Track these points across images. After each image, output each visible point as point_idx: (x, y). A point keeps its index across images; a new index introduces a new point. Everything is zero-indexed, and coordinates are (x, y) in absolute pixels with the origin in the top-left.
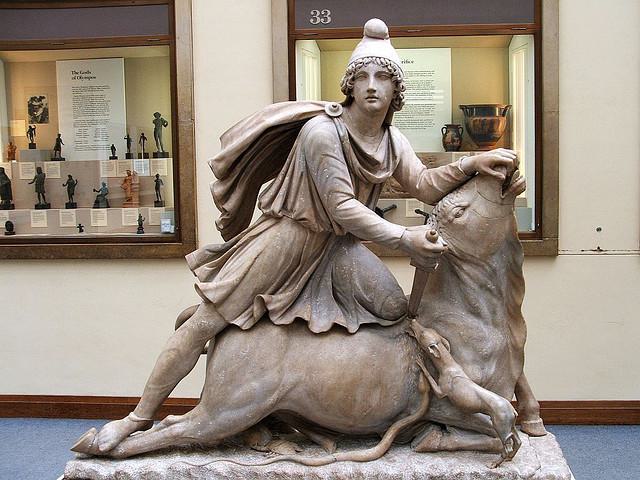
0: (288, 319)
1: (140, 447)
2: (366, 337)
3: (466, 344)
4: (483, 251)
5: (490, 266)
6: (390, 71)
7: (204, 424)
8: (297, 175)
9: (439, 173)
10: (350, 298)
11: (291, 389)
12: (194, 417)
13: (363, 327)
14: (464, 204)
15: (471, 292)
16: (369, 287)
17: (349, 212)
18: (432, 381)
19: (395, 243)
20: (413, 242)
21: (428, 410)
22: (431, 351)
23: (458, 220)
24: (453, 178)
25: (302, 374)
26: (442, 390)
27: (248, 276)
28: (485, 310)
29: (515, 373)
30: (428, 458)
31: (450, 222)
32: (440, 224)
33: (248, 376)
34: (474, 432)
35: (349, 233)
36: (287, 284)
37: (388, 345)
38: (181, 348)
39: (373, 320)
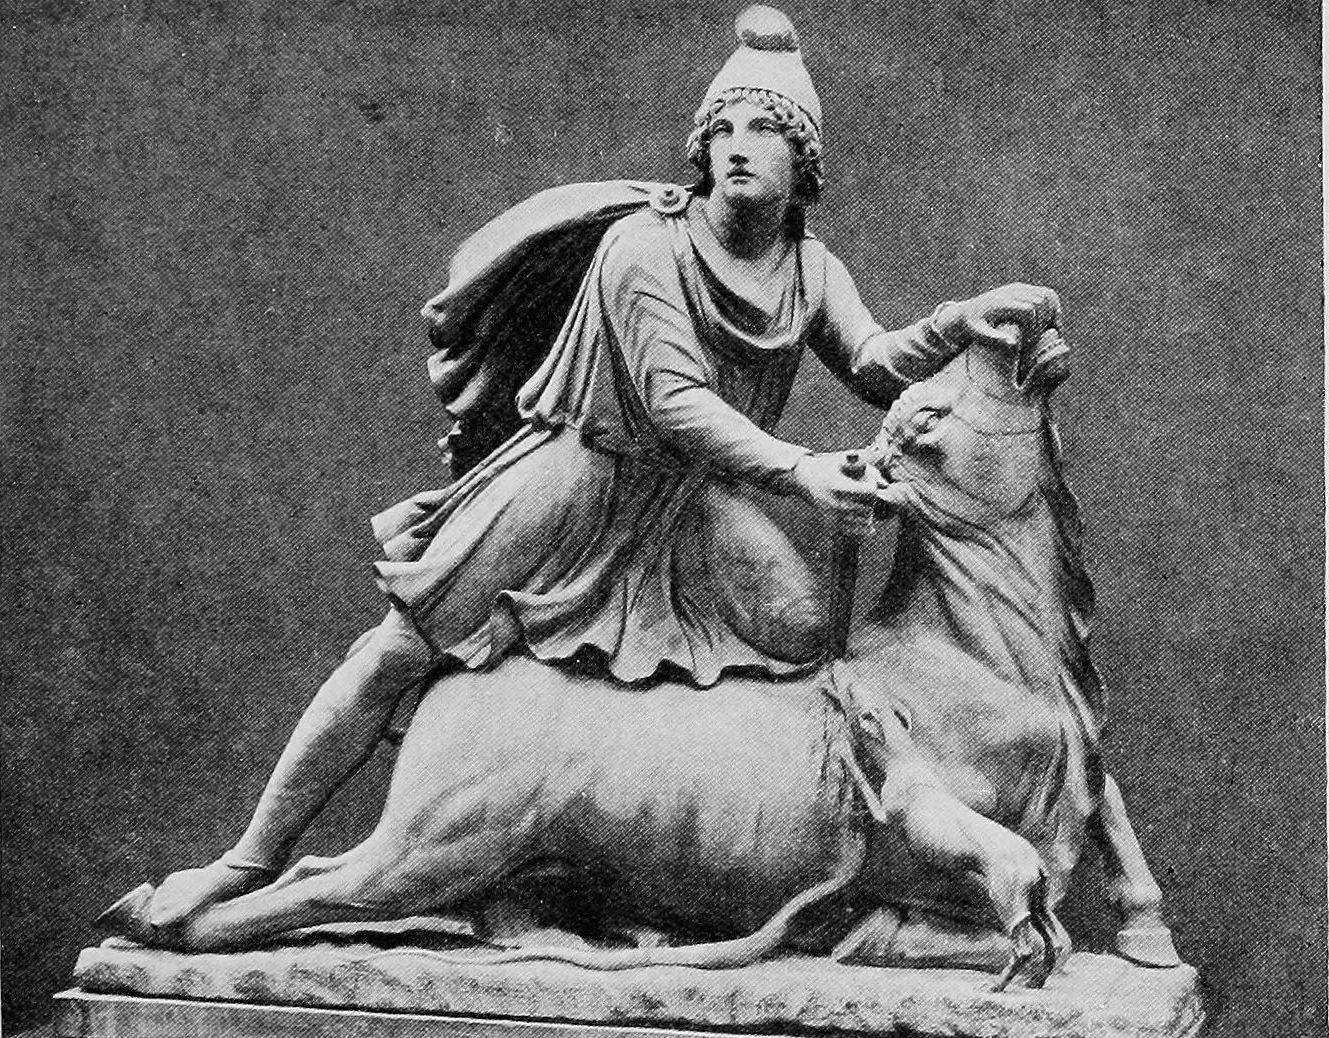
0: (565, 648)
6: (779, 118)
13: (732, 673)
18: (867, 790)
22: (865, 724)
24: (923, 351)
36: (572, 572)
39: (748, 657)
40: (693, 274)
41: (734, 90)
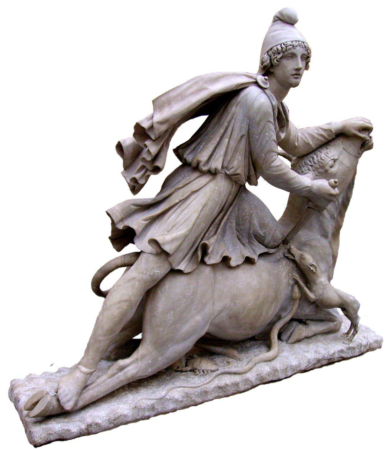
1: (97, 396)
2: (261, 263)
7: (155, 360)
8: (236, 135)
9: (314, 134)
12: (143, 357)
14: (336, 157)
15: (325, 221)
16: (264, 224)
17: (280, 168)
19: (306, 191)
23: (333, 170)
25: (227, 302)
26: (315, 295)
27: (196, 225)
30: (302, 346)
31: (326, 171)
32: (317, 173)
33: (193, 312)
34: (321, 321)
38: (132, 299)
39: (265, 250)
40: (276, 111)
41: (296, 41)
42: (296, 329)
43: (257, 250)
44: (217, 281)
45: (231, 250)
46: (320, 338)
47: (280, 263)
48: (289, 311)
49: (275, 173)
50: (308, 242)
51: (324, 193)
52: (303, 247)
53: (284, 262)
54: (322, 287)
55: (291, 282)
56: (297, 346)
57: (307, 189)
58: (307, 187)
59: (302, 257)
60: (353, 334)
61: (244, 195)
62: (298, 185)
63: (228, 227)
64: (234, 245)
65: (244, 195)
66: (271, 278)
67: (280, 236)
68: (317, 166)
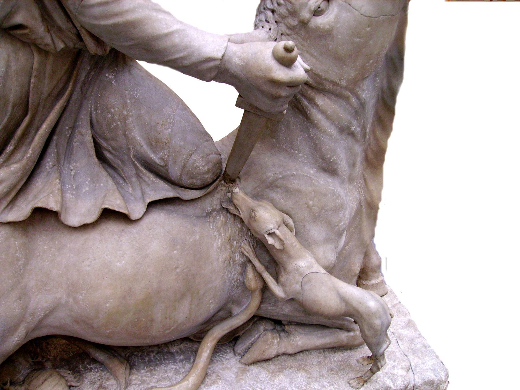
3: (316, 218)
4: (353, 74)
5: (358, 98)
10: (126, 158)
11: (46, 316)
13: (152, 205)
15: (325, 139)
16: (158, 141)
20: (246, 67)
21: (259, 308)
22: (271, 241)
23: (321, 21)
25: (61, 295)
26: (285, 292)
28: (343, 166)
29: (366, 237)
32: (283, 28)
35: (113, 50)
37: (197, 229)
42: (259, 339)
43: (149, 192)
44: (38, 254)
45: (87, 189)
46: (314, 359)
47: (212, 219)
48: (245, 306)
49: (103, 23)
50: (280, 182)
51: (257, 77)
52: (267, 190)
53: (221, 219)
54: (299, 278)
55: (239, 259)
56: (255, 369)
57: (211, 64)
58: (210, 59)
59: (252, 218)
60: (370, 369)
61: (110, 77)
62: (181, 55)
63: (77, 143)
64: (95, 180)
65: (110, 77)
66: (175, 252)
67: (203, 166)
68: (282, 10)
